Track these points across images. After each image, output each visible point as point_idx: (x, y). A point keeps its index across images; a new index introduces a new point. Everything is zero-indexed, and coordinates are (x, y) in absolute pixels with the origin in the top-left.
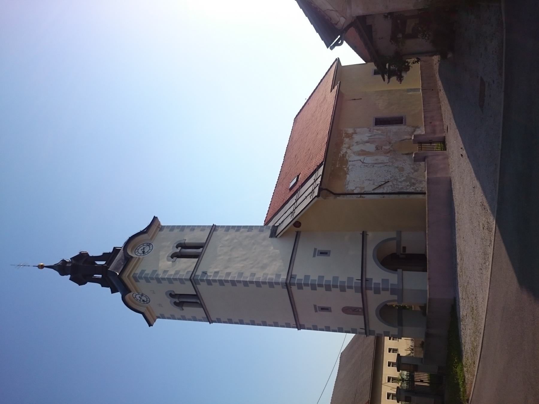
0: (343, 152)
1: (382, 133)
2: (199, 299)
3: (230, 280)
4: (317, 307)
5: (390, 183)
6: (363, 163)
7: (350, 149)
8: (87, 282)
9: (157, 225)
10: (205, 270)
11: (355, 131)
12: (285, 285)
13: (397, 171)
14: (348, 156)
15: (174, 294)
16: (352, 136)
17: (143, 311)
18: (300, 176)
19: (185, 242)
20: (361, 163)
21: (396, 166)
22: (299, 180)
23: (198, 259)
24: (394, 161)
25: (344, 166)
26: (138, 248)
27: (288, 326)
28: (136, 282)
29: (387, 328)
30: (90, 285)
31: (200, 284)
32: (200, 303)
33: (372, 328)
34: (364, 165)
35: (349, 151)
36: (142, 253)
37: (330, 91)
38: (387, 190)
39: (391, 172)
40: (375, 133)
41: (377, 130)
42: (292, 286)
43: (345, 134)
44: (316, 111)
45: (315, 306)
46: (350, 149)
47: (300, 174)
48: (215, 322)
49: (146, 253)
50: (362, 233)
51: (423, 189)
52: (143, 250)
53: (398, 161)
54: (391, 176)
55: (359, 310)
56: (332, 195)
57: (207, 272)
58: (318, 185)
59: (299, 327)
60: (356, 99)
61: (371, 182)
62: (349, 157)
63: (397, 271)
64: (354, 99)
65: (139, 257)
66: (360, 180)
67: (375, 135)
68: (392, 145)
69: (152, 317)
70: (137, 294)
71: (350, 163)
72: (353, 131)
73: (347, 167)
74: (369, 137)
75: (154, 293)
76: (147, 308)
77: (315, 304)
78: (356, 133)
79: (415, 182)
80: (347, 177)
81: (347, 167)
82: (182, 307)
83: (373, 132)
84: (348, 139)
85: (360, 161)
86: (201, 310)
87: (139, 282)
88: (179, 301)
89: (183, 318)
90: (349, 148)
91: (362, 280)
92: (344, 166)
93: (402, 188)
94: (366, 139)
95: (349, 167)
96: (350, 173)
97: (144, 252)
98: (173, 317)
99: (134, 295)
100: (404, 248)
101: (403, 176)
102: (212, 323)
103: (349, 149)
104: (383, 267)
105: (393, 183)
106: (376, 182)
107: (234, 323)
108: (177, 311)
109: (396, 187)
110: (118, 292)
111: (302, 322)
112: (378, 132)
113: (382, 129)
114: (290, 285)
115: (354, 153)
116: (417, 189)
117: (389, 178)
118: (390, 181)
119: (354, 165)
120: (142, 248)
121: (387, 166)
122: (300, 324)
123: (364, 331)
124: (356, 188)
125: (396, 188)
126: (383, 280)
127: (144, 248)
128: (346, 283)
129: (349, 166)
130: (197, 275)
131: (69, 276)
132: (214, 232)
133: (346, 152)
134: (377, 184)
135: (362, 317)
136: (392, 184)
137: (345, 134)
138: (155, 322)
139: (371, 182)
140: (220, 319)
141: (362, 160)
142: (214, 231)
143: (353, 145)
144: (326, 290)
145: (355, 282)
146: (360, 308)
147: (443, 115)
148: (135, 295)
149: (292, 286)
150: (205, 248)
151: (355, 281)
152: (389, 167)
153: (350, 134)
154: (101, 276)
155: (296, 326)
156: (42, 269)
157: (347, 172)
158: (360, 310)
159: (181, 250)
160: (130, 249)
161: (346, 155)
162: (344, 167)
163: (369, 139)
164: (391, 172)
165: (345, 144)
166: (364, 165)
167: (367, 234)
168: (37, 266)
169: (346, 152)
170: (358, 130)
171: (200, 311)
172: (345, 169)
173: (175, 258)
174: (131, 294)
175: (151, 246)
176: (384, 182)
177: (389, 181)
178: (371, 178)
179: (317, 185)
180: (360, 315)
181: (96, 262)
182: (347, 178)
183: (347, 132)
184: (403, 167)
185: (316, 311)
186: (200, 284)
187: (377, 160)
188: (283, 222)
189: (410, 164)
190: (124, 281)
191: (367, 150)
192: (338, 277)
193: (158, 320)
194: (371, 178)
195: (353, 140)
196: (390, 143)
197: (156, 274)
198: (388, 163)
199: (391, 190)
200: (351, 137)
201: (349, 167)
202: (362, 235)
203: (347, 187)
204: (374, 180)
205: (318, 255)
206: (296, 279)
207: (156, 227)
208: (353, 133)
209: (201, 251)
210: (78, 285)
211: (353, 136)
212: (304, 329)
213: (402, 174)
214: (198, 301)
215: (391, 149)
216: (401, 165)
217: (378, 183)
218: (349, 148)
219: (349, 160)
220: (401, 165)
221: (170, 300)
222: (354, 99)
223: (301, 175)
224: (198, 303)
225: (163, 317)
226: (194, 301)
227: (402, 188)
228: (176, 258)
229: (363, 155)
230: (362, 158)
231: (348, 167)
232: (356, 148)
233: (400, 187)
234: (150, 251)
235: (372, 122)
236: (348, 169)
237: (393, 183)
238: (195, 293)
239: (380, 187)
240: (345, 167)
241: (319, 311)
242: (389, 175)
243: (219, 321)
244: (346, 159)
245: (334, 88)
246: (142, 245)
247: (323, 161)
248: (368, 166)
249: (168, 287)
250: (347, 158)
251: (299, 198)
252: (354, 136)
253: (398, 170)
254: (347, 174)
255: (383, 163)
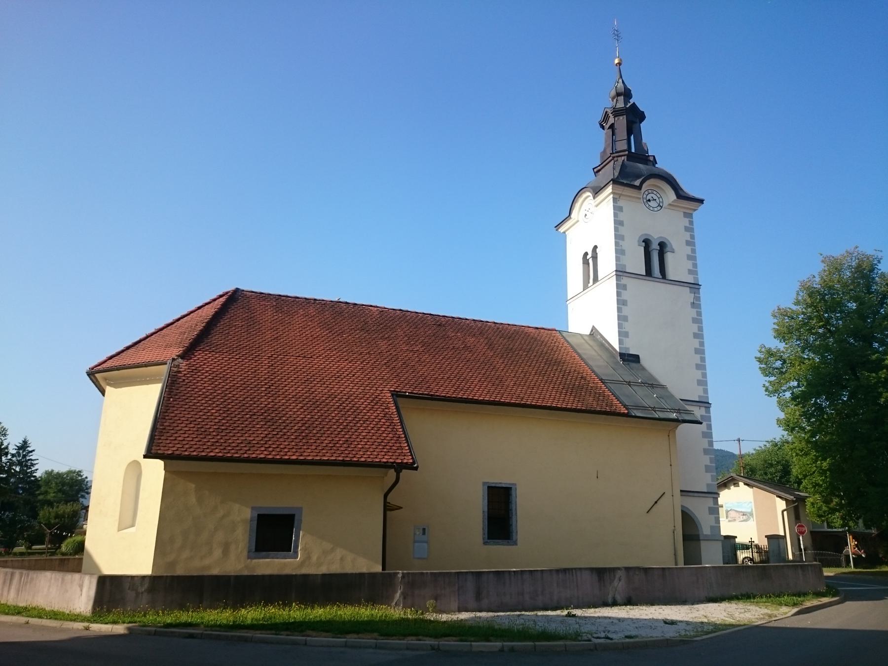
26: (655, 192)
36: (647, 199)
49: (647, 206)
52: (651, 199)
97: (649, 200)
104: (695, 519)
120: (655, 197)
127: (655, 200)
128: (712, 474)
132: (689, 288)
136: (66, 607)
142: (690, 287)
147: (355, 636)
150: (662, 280)
175: (659, 208)
190: (631, 188)
206: (706, 414)
207: (620, 192)
209: (655, 276)
228: (659, 249)
234: (651, 209)
246: (659, 196)
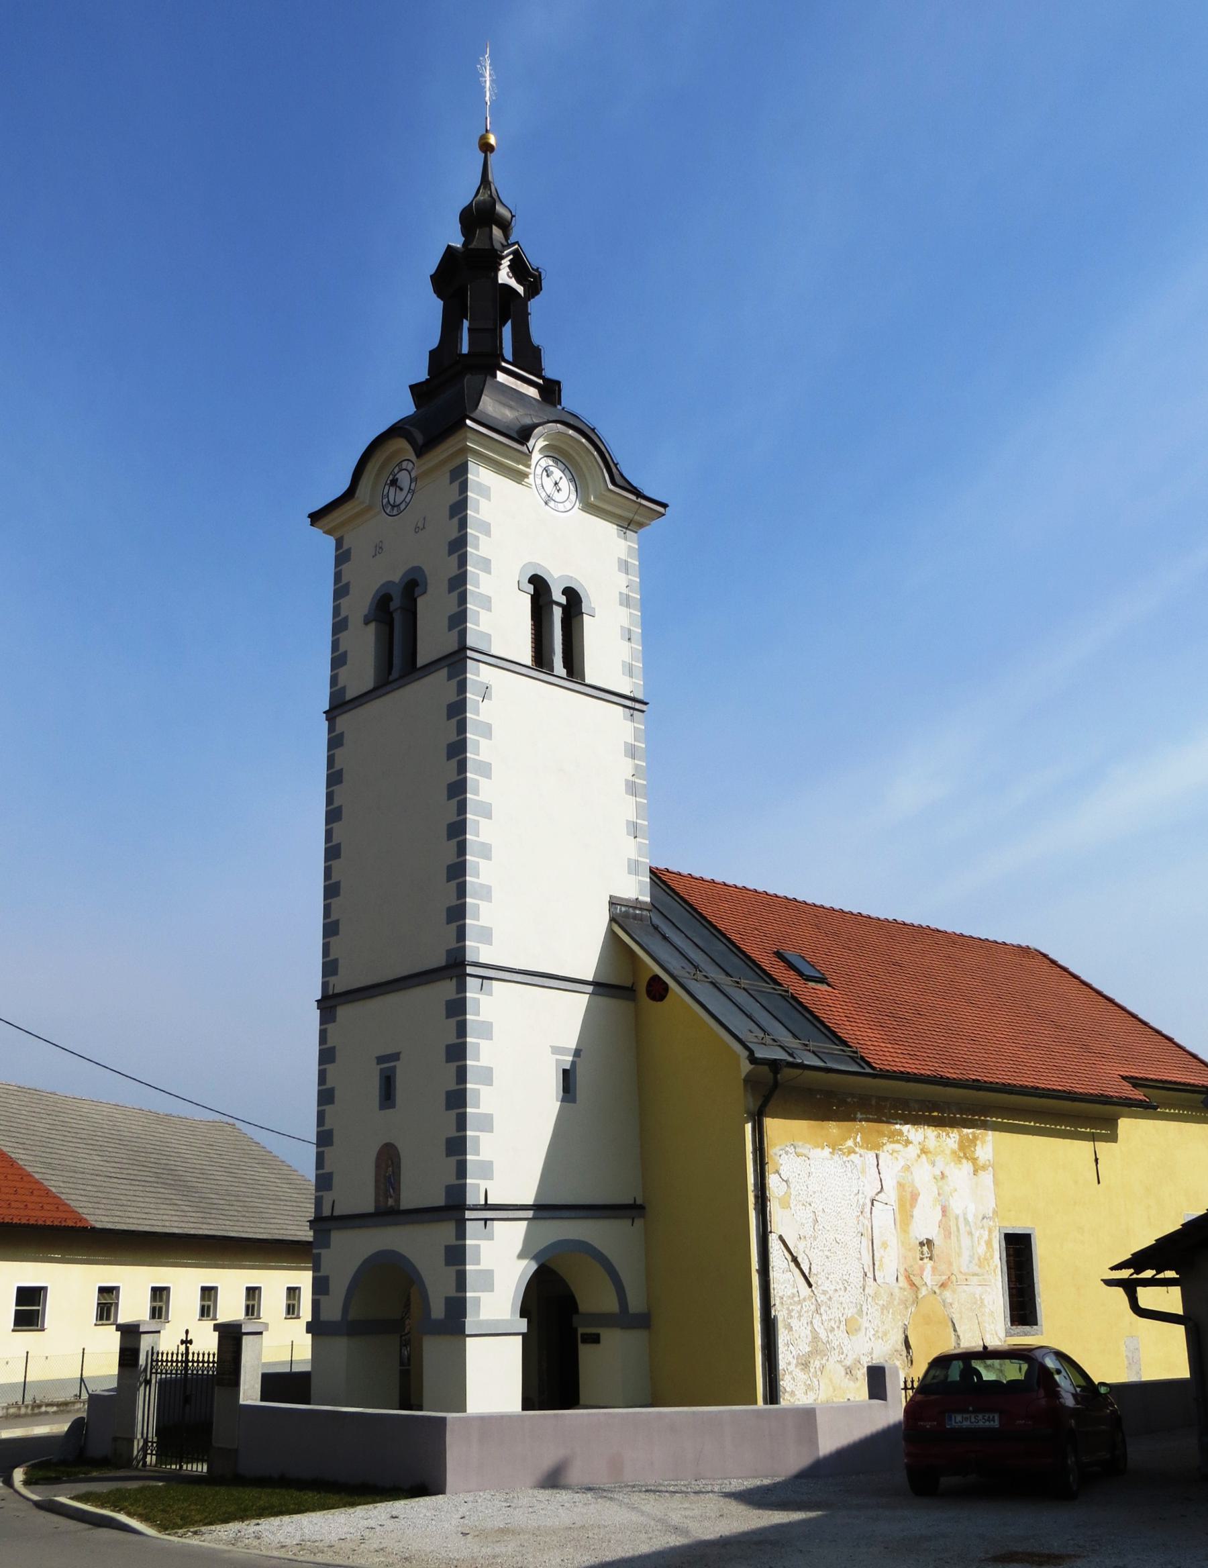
0: (909, 1131)
1: (976, 1261)
2: (401, 677)
3: (465, 778)
4: (392, 1064)
5: (804, 1290)
6: (872, 1202)
7: (919, 1156)
8: (442, 299)
9: (637, 518)
10: (494, 691)
11: (984, 1168)
12: (458, 961)
13: (846, 1310)
14: (894, 1151)
15: (416, 595)
16: (967, 1158)
17: (357, 495)
18: (824, 987)
19: (584, 615)
20: (872, 1194)
21: (864, 1309)
22: (811, 984)
23: (529, 663)
24: (881, 1302)
25: (859, 1139)
27: (330, 968)
28: (452, 472)
29: (339, 1287)
30: (435, 306)
31: (450, 678)
32: (391, 678)
33: (339, 1238)
34: (864, 1205)
35: (913, 1150)
37: (1126, 1074)
38: (782, 1281)
39: (842, 1293)
40: (977, 1234)
41: (989, 1243)
42: (454, 980)
43: (971, 1136)
44: (1057, 1027)
45: (396, 1057)
46: (919, 1156)
47: (829, 985)
48: (331, 729)
50: (639, 1202)
51: (787, 1396)
53: (882, 1313)
54: (831, 1292)
55: (391, 1197)
56: (759, 1103)
57: (490, 699)
58: (823, 974)
59: (329, 1004)
60: (1097, 1163)
61: (807, 1230)
62: (891, 1154)
63: (522, 1316)
64: (1096, 1160)
65: (530, 474)
66: (814, 1192)
67: (970, 1233)
68: (937, 1291)
69: (343, 524)
70: (413, 475)
71: (870, 1156)
72: (981, 1161)
73: (857, 1149)
74: (965, 1214)
75: (417, 529)
76: (370, 508)
77: (401, 1056)
78: (975, 1172)
79: (812, 1370)
80: (823, 1148)
81: (857, 1149)
82: (375, 620)
83: (983, 1227)
84: (955, 1146)
85: (879, 1190)
86: (368, 683)
87: (451, 482)
88: (396, 609)
89: (339, 626)
90: (924, 1151)
91: (487, 1207)
92: (859, 1139)
93: (791, 1329)
94: (956, 1207)
95: (858, 1155)
96: (836, 1157)
98: (341, 591)
99: (410, 466)
100: (595, 1339)
101: (832, 1330)
102: (327, 719)
103: (919, 1152)
105: (804, 1300)
106: (809, 1245)
107: (329, 827)
108: (360, 603)
109: (793, 1310)
110: (416, 407)
111: (344, 1012)
112: (983, 1243)
113: (992, 1258)
114: (457, 976)
115: (907, 1168)
116: (787, 1377)
117: (822, 1288)
118: (812, 1291)
119: (863, 1172)
121: (864, 1280)
122: (335, 1007)
123: (326, 1212)
124: (786, 1181)
125: (788, 1309)
126: (490, 1273)
129: (861, 1156)
130: (478, 669)
131: (459, 245)
133: (908, 1142)
134: (801, 1250)
135: (370, 1208)
137: (971, 1136)
138: (324, 532)
139: (807, 1230)
140: (344, 663)
141: (881, 1197)
143: (933, 1164)
144: (447, 1093)
145: (478, 1185)
146: (398, 1201)
148: (409, 468)
149: (454, 980)
151: (483, 1184)
152: (861, 1284)
153: (974, 1152)
154: (465, 349)
155: (331, 993)
156: (477, 146)
157: (840, 1150)
158: (391, 1202)
159: (558, 604)
160: (554, 443)
161: (898, 1142)
162: (855, 1139)
163: (957, 1218)
164: (842, 1293)
165: (938, 1136)
166: (864, 1205)
167: (636, 1221)
168: (485, 181)
169: (908, 1142)
170: (986, 1177)
171: (361, 676)
172: (850, 1143)
173: (531, 588)
174: (413, 458)
176: (807, 1274)
177: (813, 1288)
178: (821, 1227)
179: (791, 1052)
180: (377, 1201)
181: (509, 324)
182: (819, 1150)
183: (978, 1142)
184: (860, 1329)
185: (381, 1060)
186: (450, 678)
187: (885, 1245)
188: (665, 938)
189: (871, 1353)
191: (916, 1212)
192: (490, 1129)
193: (330, 542)
194: (821, 1227)
195: (953, 1164)
196: (943, 1285)
197: (477, 534)
198: (875, 1280)
199: (781, 1294)
200: (962, 1155)
201: (858, 1155)
202: (631, 1202)
203: (787, 1153)
204: (815, 1238)
205: (557, 1060)
208: (974, 1160)
210: (433, 271)
211: (964, 1161)
212: (322, 1022)
213: (838, 1327)
214: (395, 674)
215: (924, 1291)
216: (868, 1325)
217: (804, 1252)
218: (924, 1151)
219: (880, 1152)
220: (868, 1325)
221: (397, 579)
222: (1096, 1160)
223: (830, 989)
224: (390, 673)
225: (342, 557)
226: (397, 661)
227: (790, 1328)
228: (532, 593)
229: (901, 1201)
230: (891, 1194)
231: (855, 1152)
232: (923, 1175)
233: (794, 1323)
235: (1018, 1227)
236: (851, 1151)
237: (804, 1300)
238: (419, 664)
239: (789, 1258)
240: (855, 1144)
241: (381, 1070)
242: (833, 1288)
243: (335, 742)
244: (884, 1144)
245: (1135, 1086)
247: (874, 1068)
248: (861, 1218)
249: (438, 574)
250: (890, 1147)
251: (749, 993)
252: (967, 1166)
253: (849, 1315)
254: (834, 1149)
255: (874, 1264)
